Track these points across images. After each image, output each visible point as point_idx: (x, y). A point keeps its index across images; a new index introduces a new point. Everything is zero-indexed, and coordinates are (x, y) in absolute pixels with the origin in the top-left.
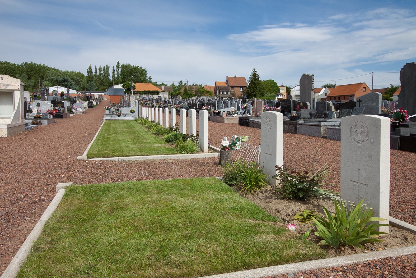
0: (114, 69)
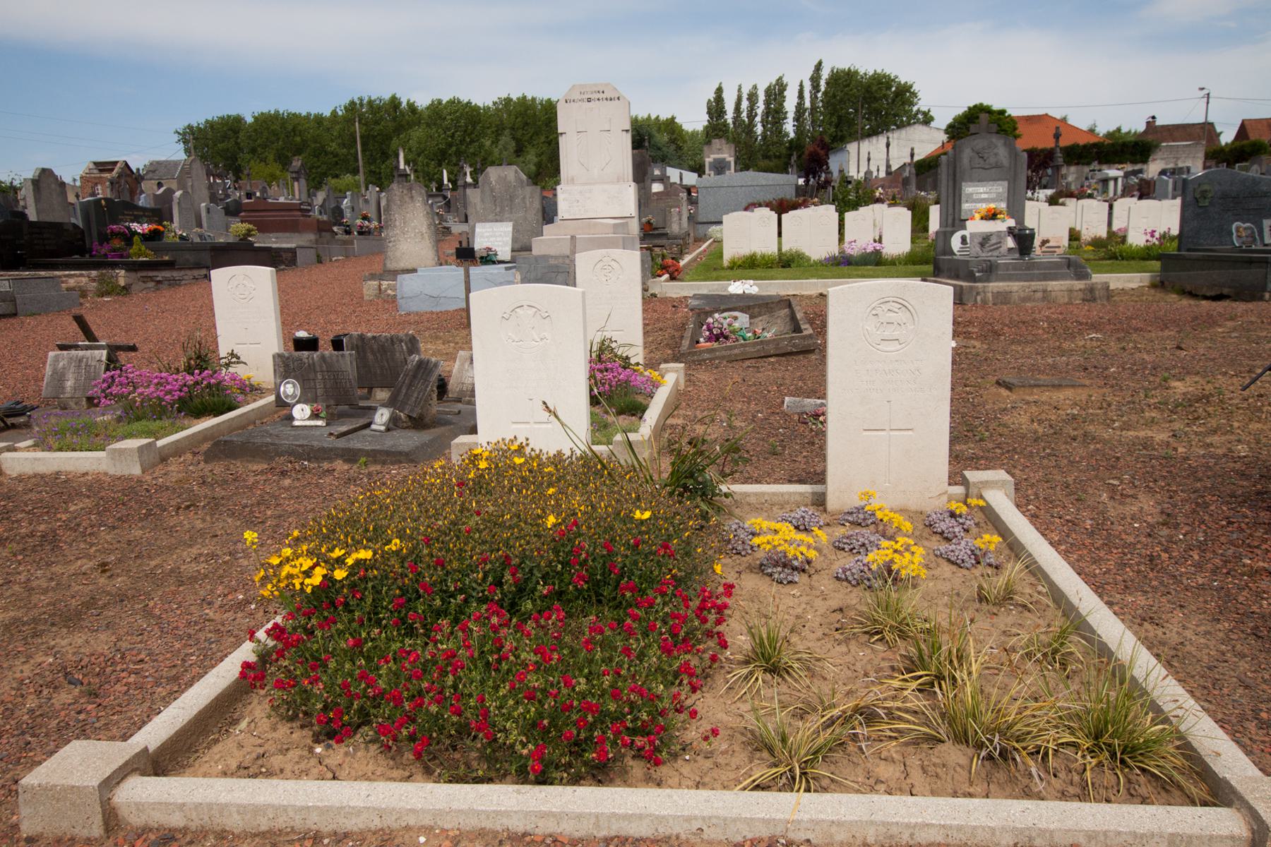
0: (801, 96)
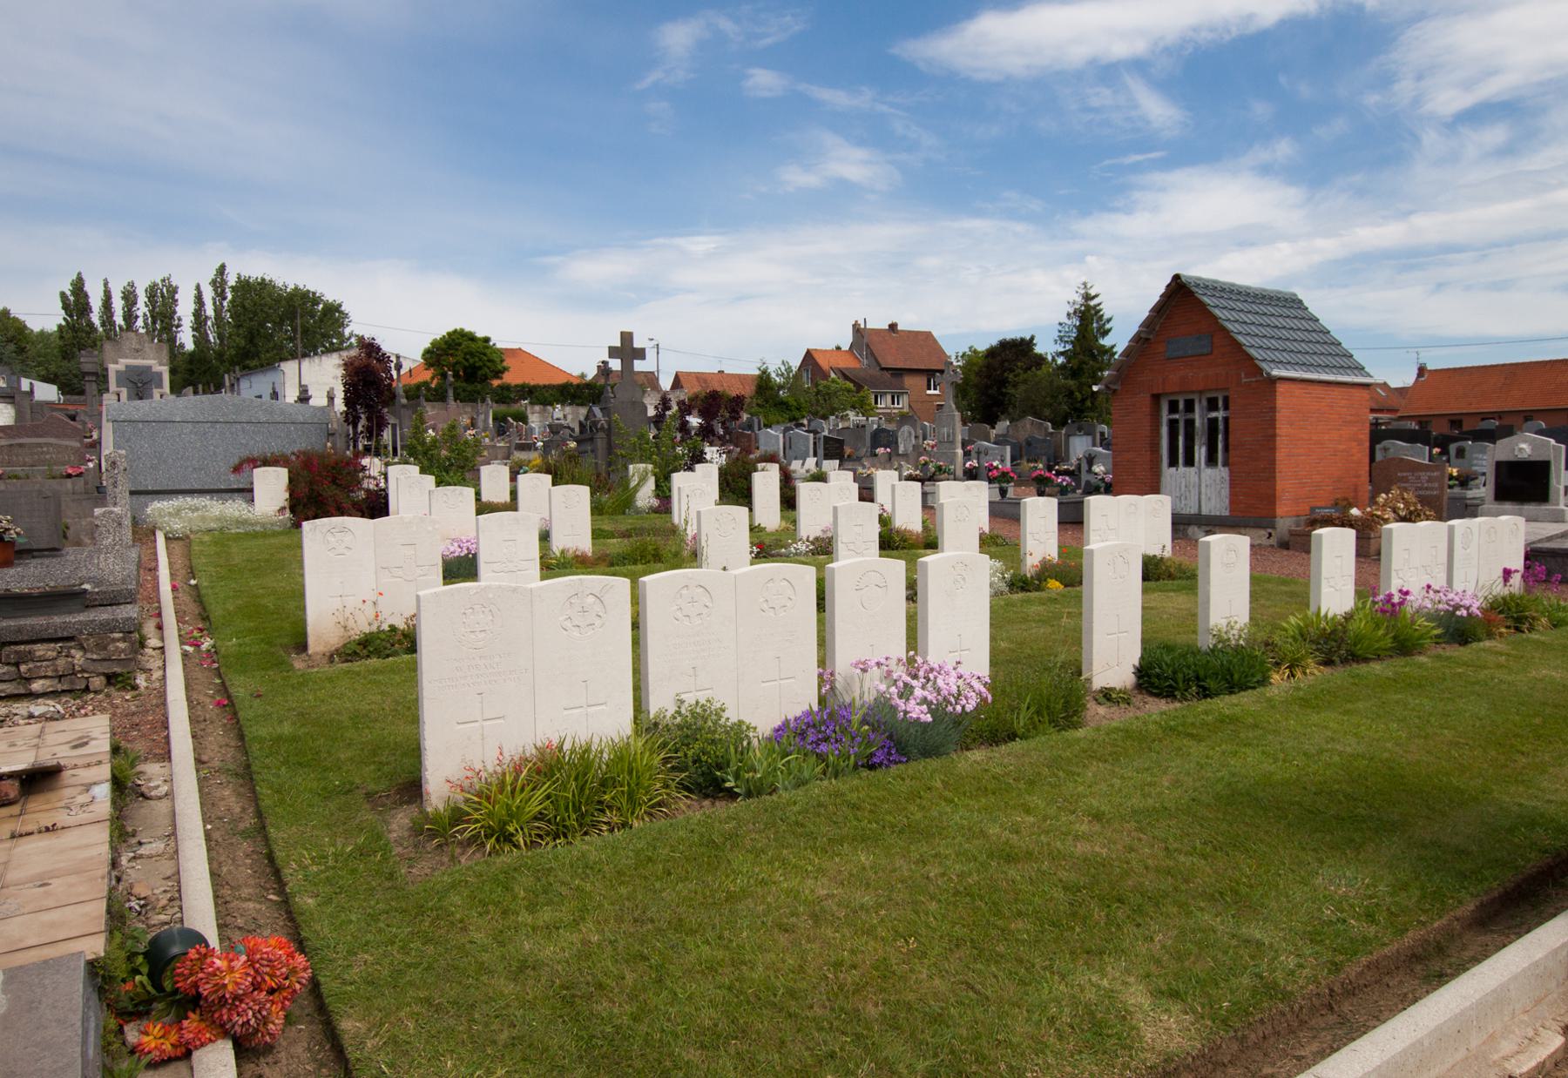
0: (199, 299)
